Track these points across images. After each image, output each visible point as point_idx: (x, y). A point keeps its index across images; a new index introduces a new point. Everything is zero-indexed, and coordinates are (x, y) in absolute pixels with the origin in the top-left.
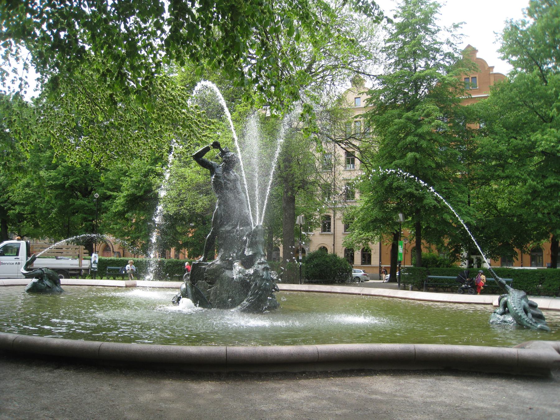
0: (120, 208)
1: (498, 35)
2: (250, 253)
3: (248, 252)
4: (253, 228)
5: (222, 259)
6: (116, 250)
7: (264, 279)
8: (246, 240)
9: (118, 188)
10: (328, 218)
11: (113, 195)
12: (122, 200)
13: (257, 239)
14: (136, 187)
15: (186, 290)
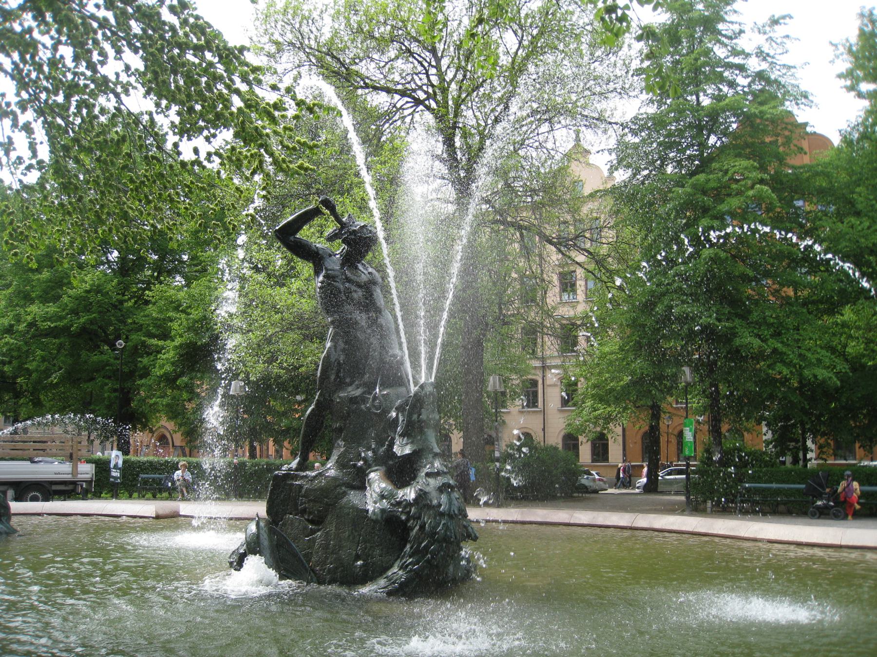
0: (168, 368)
2: (407, 450)
3: (402, 448)
4: (413, 389)
5: (341, 464)
7: (442, 514)
10: (534, 383)
12: (172, 353)
13: (423, 417)
15: (257, 536)
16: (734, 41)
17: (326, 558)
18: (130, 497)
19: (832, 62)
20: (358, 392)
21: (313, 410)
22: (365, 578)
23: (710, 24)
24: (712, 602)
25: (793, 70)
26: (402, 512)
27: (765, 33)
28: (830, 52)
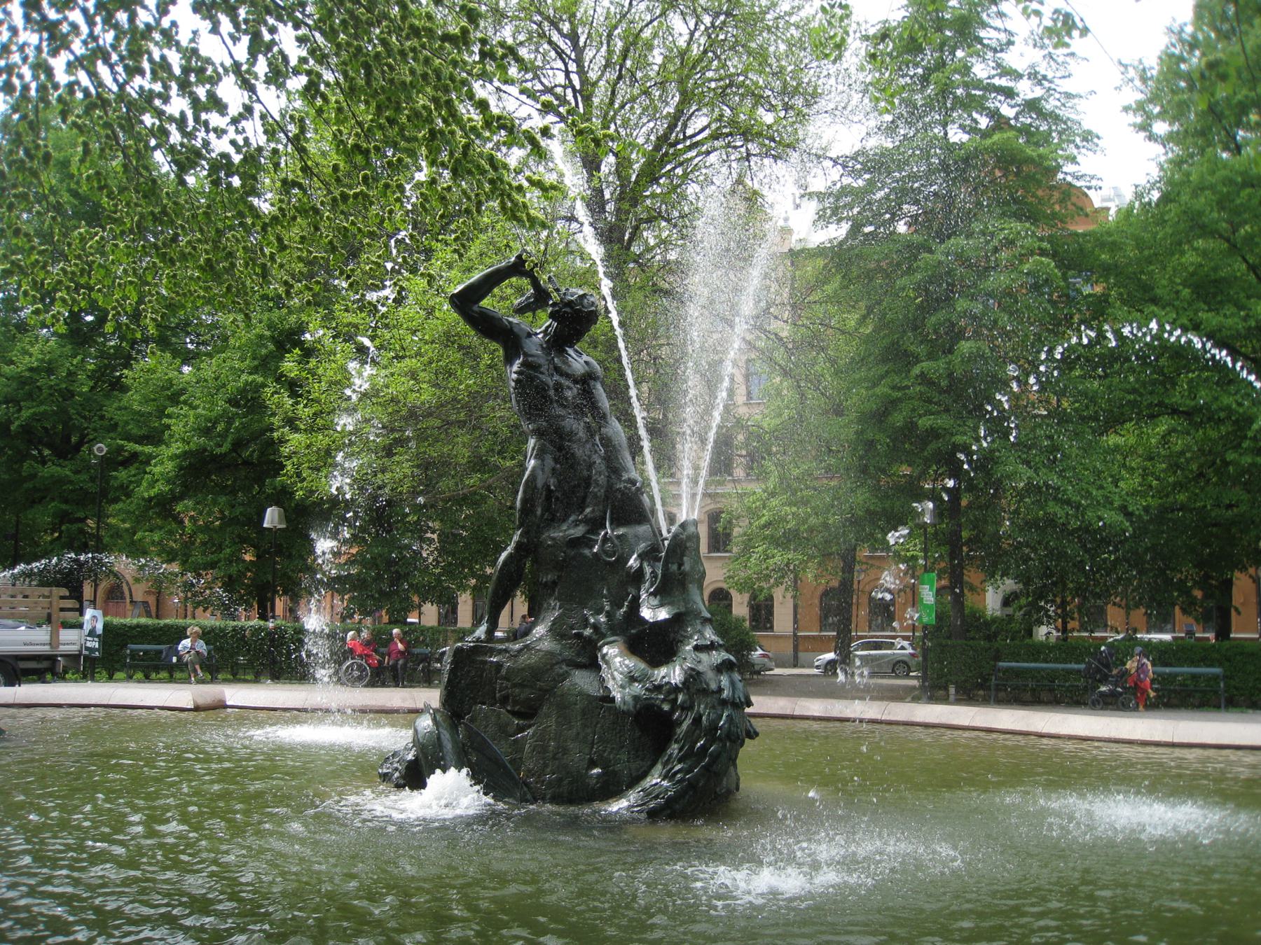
0: (161, 487)
1: (1130, 69)
2: (663, 614)
5: (557, 632)
6: (139, 597)
7: (724, 703)
8: (641, 569)
9: (155, 437)
11: (143, 453)
12: (170, 466)
14: (206, 432)
16: (999, 55)
17: (546, 766)
18: (110, 678)
19: (1118, 88)
20: (579, 531)
21: (510, 556)
22: (611, 789)
23: (966, 29)
25: (1076, 101)
26: (663, 701)
27: (1042, 47)
28: (1116, 76)
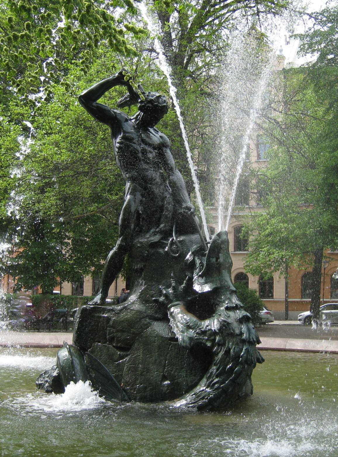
2: (207, 288)
5: (143, 299)
7: (244, 341)
17: (136, 379)
20: (156, 238)
21: (115, 253)
24: (333, 419)
26: (207, 340)
